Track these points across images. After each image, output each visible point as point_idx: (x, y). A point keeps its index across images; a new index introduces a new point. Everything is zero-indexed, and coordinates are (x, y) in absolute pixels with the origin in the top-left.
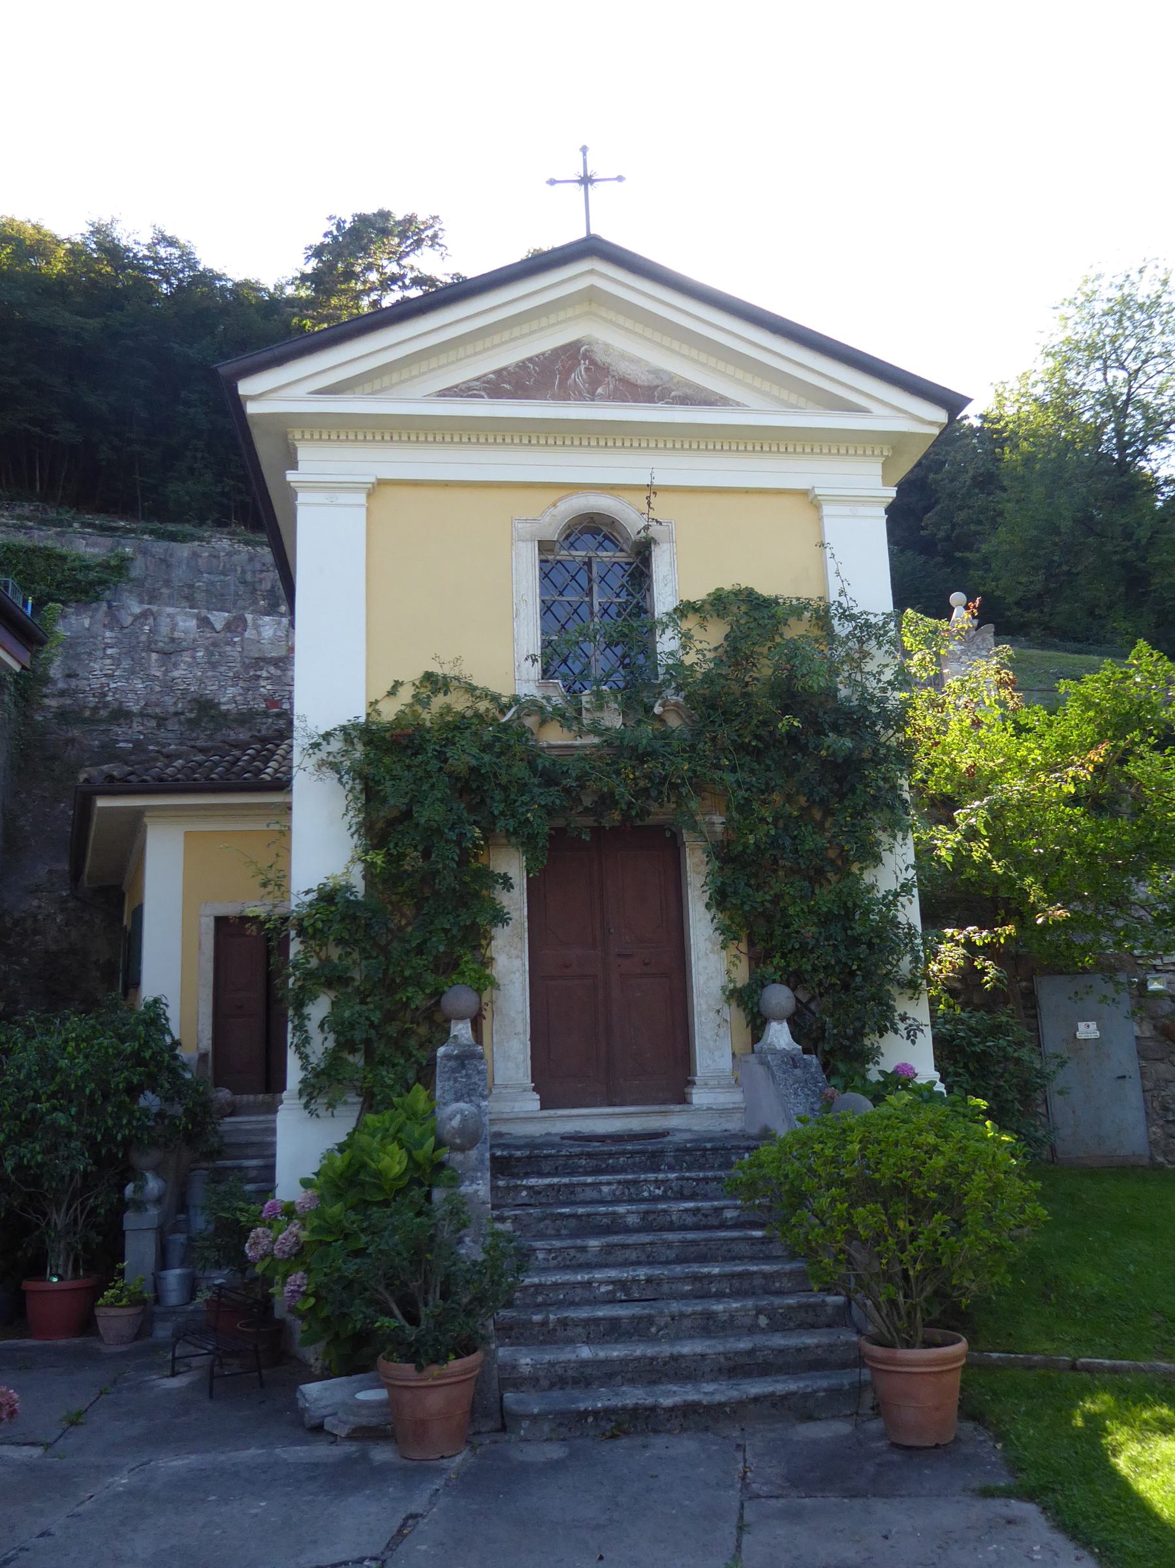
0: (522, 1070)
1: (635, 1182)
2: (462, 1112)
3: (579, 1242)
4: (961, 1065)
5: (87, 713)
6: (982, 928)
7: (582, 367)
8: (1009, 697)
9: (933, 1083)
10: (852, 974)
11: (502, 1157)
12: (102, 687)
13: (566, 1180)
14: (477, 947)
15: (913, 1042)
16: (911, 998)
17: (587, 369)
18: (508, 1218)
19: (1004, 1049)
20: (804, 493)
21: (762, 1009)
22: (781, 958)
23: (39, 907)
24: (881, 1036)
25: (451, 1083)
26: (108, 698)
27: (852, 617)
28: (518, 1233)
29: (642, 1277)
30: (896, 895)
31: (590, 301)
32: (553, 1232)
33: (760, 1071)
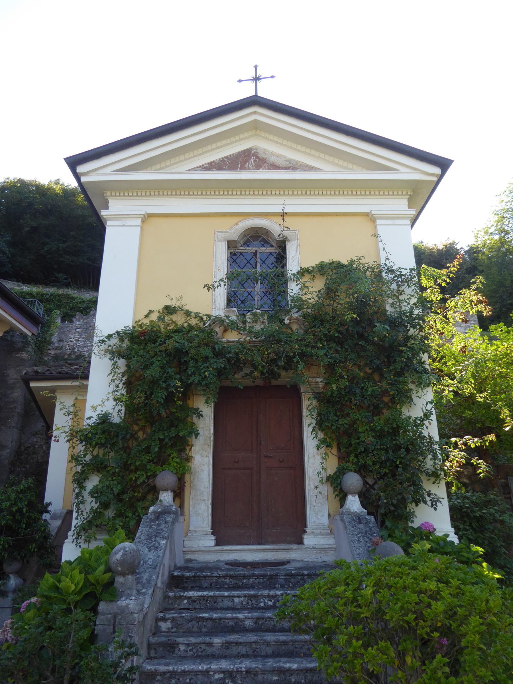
0: (206, 522)
1: (255, 596)
2: (125, 548)
3: (208, 639)
4: (468, 524)
5: (66, 357)
6: (474, 437)
7: (252, 160)
8: (483, 309)
9: (447, 535)
10: (397, 467)
11: (177, 576)
12: (73, 345)
13: (211, 593)
14: (183, 450)
15: (435, 509)
16: (434, 483)
17: (255, 161)
18: (169, 619)
19: (492, 515)
20: (367, 215)
21: (343, 488)
22: (354, 457)
23: (37, 442)
24: (417, 505)
25: (147, 529)
26: (76, 350)
27: (392, 271)
28: (174, 630)
29: (243, 669)
30: (422, 420)
31: (256, 129)
32: (197, 630)
33: (340, 524)
